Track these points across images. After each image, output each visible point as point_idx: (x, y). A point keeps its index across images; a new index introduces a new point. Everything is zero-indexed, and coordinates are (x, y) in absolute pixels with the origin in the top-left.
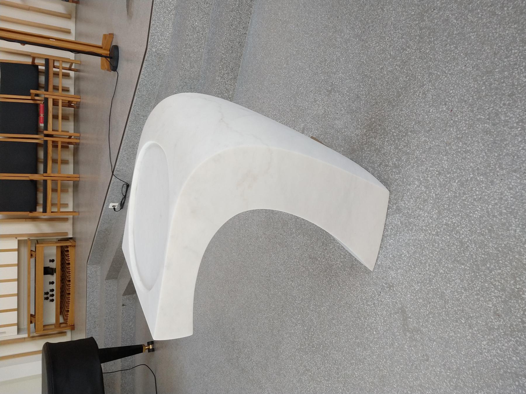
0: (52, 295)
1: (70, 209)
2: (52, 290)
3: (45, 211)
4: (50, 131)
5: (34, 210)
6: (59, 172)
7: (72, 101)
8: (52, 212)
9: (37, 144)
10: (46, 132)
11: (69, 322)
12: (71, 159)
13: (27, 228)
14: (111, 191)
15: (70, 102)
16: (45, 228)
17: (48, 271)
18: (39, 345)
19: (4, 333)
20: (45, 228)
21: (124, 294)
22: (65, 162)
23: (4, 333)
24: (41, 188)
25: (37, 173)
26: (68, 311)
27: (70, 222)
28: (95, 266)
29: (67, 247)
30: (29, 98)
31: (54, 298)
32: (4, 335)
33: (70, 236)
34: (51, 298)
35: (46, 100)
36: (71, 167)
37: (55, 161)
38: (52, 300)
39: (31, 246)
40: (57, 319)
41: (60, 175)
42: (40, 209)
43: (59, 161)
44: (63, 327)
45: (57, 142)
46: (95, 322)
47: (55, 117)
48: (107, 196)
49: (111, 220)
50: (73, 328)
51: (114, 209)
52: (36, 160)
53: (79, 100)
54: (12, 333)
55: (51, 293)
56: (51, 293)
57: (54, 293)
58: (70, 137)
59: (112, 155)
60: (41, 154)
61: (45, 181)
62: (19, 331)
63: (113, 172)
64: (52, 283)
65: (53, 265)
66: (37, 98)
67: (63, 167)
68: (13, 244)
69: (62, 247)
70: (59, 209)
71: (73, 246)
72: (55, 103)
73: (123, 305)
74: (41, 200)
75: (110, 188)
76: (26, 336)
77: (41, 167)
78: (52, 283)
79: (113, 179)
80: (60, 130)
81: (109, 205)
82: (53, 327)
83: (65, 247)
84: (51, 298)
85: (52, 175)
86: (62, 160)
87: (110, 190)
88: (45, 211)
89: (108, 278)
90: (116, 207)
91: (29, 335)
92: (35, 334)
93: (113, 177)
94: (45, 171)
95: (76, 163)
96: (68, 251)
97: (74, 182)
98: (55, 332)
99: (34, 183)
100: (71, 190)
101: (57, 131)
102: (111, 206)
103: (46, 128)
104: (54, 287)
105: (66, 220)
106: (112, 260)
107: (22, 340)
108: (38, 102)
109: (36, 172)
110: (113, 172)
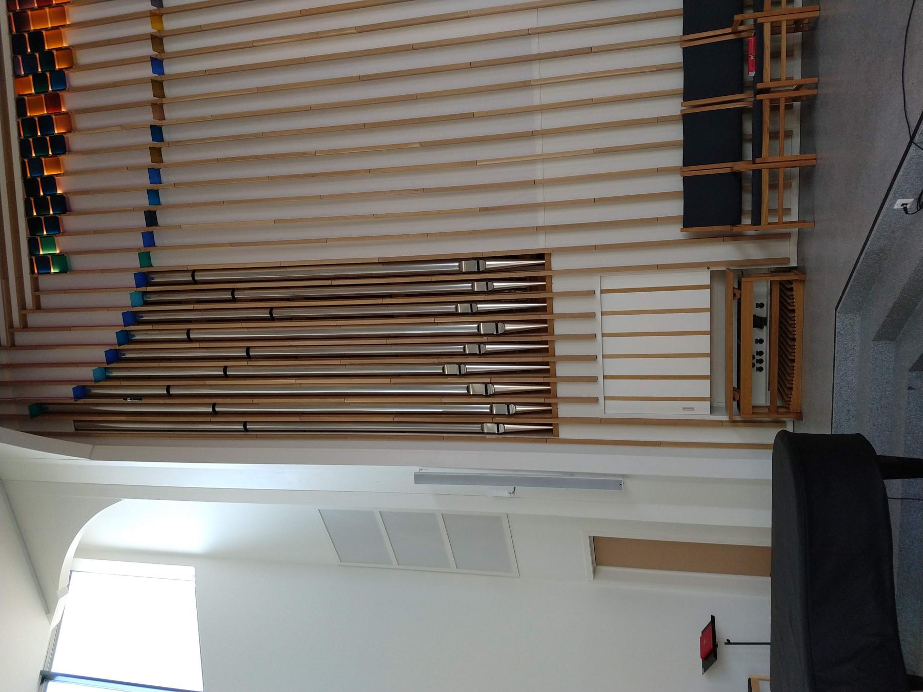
0: (761, 361)
1: (794, 217)
2: (761, 353)
3: (757, 221)
4: (767, 83)
5: (737, 221)
6: (781, 151)
7: (804, 19)
8: (769, 224)
9: (741, 110)
10: (760, 86)
11: (793, 406)
12: (796, 127)
13: (724, 253)
14: (903, 175)
15: (797, 22)
16: (752, 252)
17: (759, 322)
18: (769, 435)
19: (693, 409)
20: (752, 252)
21: (912, 369)
22: (789, 135)
23: (693, 409)
24: (747, 185)
25: (741, 160)
26: (791, 389)
27: (795, 239)
28: (850, 315)
29: (790, 282)
30: (729, 30)
31: (763, 365)
32: (691, 412)
33: (794, 264)
34: (758, 365)
35: (759, 28)
36: (796, 141)
37: (774, 136)
38: (760, 369)
39: (732, 280)
40: (773, 401)
41: (783, 159)
42: (747, 221)
43: (782, 134)
44: (782, 413)
45: (778, 100)
46: (848, 411)
47: (776, 55)
48: (895, 186)
49: (893, 232)
50: (799, 416)
51: (905, 210)
52: (740, 138)
53: (817, 14)
54: (702, 411)
55: (758, 357)
56: (758, 357)
57: (763, 357)
58: (799, 88)
59: (909, 106)
60: (748, 128)
61: (758, 173)
62: (713, 410)
63: (912, 138)
64: (761, 341)
65: (763, 313)
66: (741, 28)
67: (788, 142)
68: (704, 278)
69: (781, 283)
70: (780, 219)
71: (800, 281)
72: (776, 30)
73: (910, 388)
74: (747, 205)
75: (902, 169)
76: (725, 418)
77: (748, 149)
78: (761, 341)
79: (911, 151)
80: (784, 78)
81: (894, 203)
82: (766, 410)
83: (787, 283)
84: (758, 365)
85: (770, 160)
86: (785, 132)
87: (901, 173)
88: (757, 221)
89: (880, 336)
90: (908, 206)
91: (730, 418)
92: (738, 418)
93: (913, 147)
94: (757, 153)
95: (808, 134)
96: (792, 289)
97: (802, 169)
98: (767, 419)
99: (737, 176)
100: (795, 184)
101: (779, 80)
102: (898, 205)
103: (759, 77)
104: (763, 347)
105: (786, 236)
106: (890, 305)
107: (719, 424)
108: (743, 35)
109: (739, 157)
110: (912, 138)
